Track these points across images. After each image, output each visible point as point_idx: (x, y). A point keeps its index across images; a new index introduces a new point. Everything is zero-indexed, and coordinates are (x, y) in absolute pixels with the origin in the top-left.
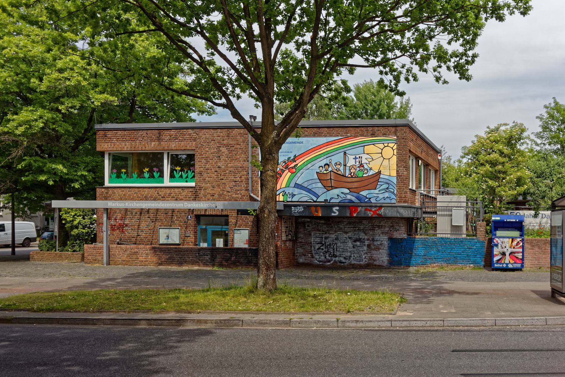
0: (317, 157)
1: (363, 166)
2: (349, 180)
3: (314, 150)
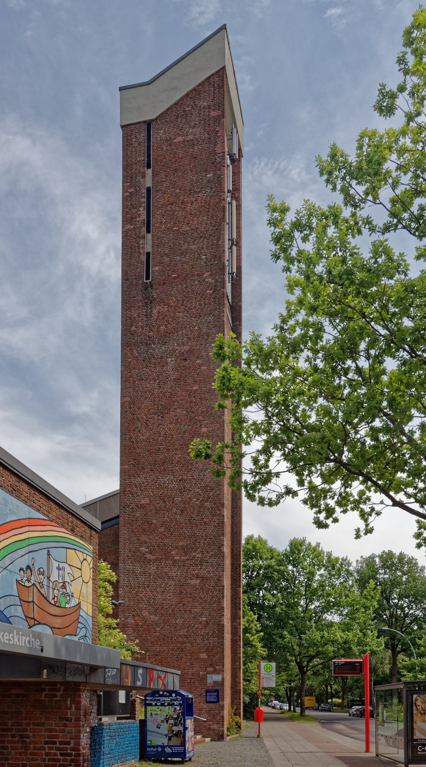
0: (14, 547)
1: (65, 588)
2: (53, 610)
3: (14, 525)
